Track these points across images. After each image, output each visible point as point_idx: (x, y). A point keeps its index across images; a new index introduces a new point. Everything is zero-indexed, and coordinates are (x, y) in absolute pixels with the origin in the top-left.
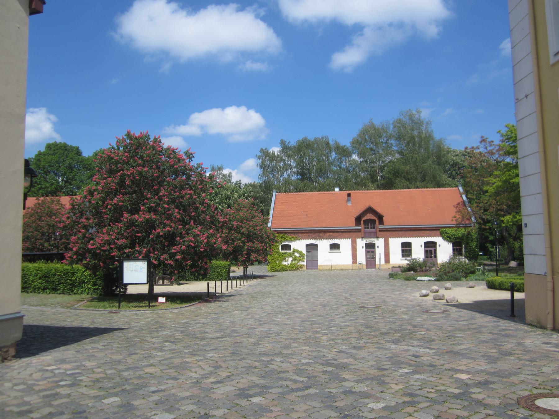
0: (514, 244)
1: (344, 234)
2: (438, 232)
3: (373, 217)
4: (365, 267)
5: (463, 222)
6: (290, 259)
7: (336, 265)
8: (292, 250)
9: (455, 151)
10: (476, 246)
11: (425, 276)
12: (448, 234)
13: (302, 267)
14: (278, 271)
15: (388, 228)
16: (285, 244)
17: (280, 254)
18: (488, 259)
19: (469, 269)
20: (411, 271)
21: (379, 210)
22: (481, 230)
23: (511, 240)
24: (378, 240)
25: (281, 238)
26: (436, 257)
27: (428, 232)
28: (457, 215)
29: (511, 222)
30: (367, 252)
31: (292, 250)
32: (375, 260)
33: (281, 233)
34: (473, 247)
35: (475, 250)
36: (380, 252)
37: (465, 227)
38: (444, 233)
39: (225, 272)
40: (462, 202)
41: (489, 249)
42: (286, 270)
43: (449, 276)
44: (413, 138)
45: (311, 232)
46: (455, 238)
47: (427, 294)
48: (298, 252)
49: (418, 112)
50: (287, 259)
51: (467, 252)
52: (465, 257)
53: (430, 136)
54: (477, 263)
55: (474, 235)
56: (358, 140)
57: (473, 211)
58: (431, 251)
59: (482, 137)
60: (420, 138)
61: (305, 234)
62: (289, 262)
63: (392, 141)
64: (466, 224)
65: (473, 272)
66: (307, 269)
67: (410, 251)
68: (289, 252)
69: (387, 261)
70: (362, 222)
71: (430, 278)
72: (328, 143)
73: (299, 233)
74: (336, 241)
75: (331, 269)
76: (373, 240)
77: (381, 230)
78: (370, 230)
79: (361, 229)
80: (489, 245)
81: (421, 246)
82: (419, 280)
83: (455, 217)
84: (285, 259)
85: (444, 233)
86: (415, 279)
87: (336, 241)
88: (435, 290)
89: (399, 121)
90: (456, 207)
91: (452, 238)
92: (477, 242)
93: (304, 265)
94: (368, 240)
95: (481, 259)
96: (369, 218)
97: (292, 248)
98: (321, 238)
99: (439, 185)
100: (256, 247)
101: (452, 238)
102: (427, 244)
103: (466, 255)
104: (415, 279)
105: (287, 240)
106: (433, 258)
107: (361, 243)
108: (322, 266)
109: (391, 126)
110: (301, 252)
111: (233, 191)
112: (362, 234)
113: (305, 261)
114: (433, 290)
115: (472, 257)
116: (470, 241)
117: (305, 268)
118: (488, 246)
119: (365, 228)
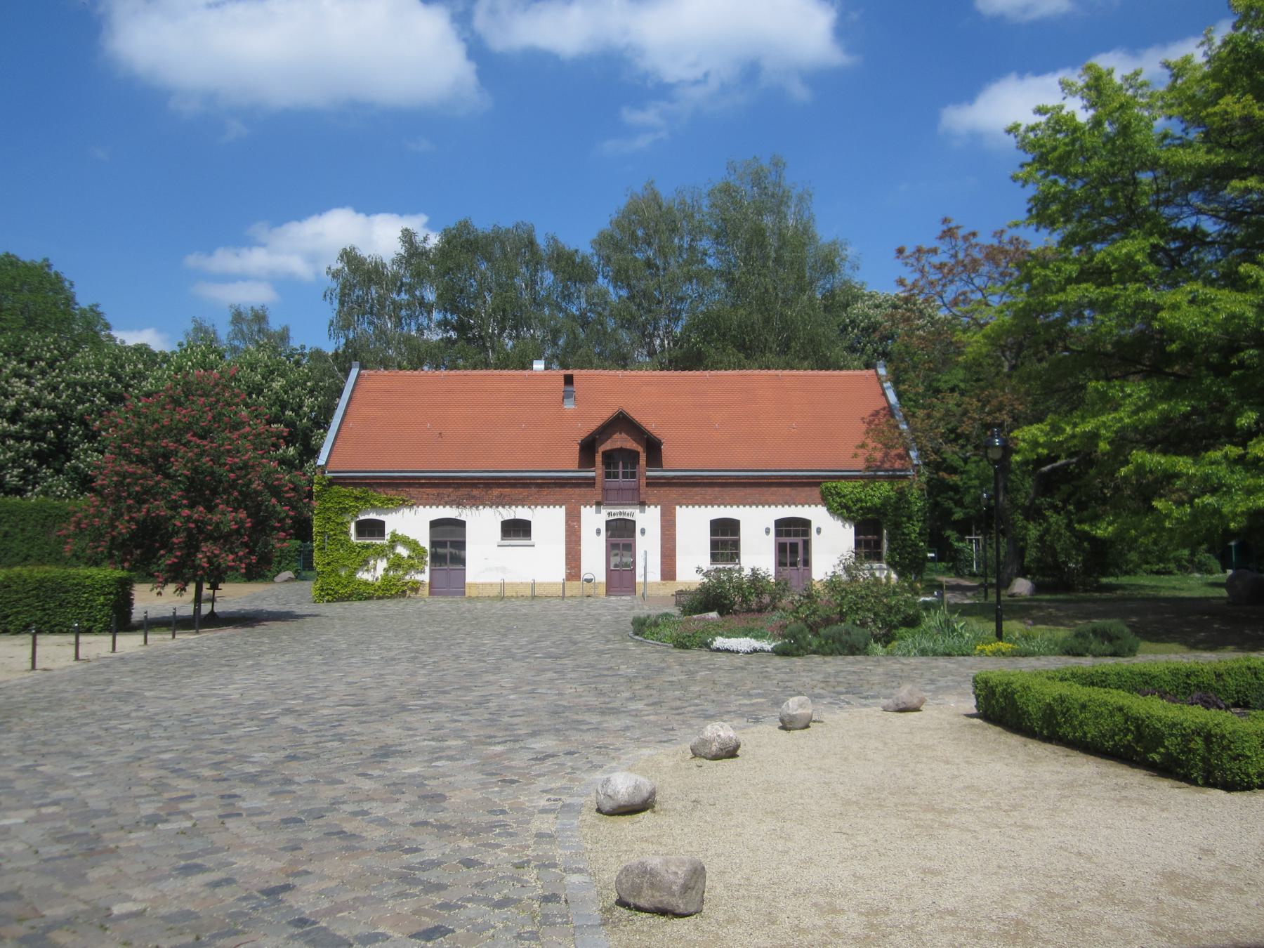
0: (1026, 528)
1: (545, 491)
2: (816, 492)
3: (630, 444)
4: (603, 590)
5: (887, 466)
6: (382, 565)
7: (517, 585)
8: (387, 537)
9: (872, 296)
10: (920, 534)
11: (746, 634)
12: (844, 496)
13: (416, 587)
14: (342, 599)
15: (673, 478)
16: (367, 517)
17: (352, 549)
18: (949, 569)
19: (898, 612)
20: (712, 610)
21: (651, 425)
22: (936, 488)
23: (1019, 518)
24: (643, 511)
25: (357, 499)
26: (807, 562)
27: (787, 490)
28: (869, 441)
29: (1043, 446)
30: (612, 547)
31: (387, 537)
32: (634, 569)
33: (356, 485)
34: (913, 536)
35: (917, 545)
36: (648, 547)
37: (891, 478)
38: (831, 494)
39: (103, 605)
40: (884, 409)
41: (951, 545)
42: (369, 598)
43: (827, 638)
44: (759, 232)
45: (448, 485)
46: (861, 508)
47: (638, 800)
48: (406, 542)
49: (776, 165)
50: (372, 562)
51: (895, 549)
52: (888, 563)
53: (806, 230)
54: (921, 582)
55: (917, 502)
56: (612, 237)
57: (913, 430)
58: (794, 547)
59: (945, 221)
60: (781, 235)
61: (428, 490)
62: (380, 572)
63: (705, 243)
64: (894, 470)
65: (912, 622)
66: (431, 593)
67: (736, 544)
68: (378, 542)
69: (668, 572)
70: (599, 458)
71: (757, 644)
72: (531, 243)
73: (410, 485)
74: (520, 513)
75: (502, 595)
76: (628, 510)
77: (653, 483)
78: (621, 481)
79: (593, 478)
80: (951, 534)
81: (768, 531)
82: (718, 650)
83: (863, 446)
84: (366, 562)
85: (831, 494)
86: (707, 645)
87: (520, 513)
88: (715, 747)
89: (727, 190)
90: (870, 423)
91: (854, 508)
92: (924, 521)
93: (422, 583)
94: (613, 511)
95: (932, 570)
96: (618, 445)
97: (388, 530)
98: (475, 502)
99: (824, 364)
100: (218, 524)
101: (854, 508)
102: (785, 527)
103: (893, 558)
104: (707, 645)
105: (373, 507)
106: (800, 566)
107: (594, 520)
108: (476, 585)
109: (705, 203)
110: (416, 543)
111: (272, 372)
112: (597, 493)
113: (427, 569)
114: (705, 742)
115: (909, 564)
116: (905, 519)
117: (425, 591)
118: (948, 537)
119: (608, 475)
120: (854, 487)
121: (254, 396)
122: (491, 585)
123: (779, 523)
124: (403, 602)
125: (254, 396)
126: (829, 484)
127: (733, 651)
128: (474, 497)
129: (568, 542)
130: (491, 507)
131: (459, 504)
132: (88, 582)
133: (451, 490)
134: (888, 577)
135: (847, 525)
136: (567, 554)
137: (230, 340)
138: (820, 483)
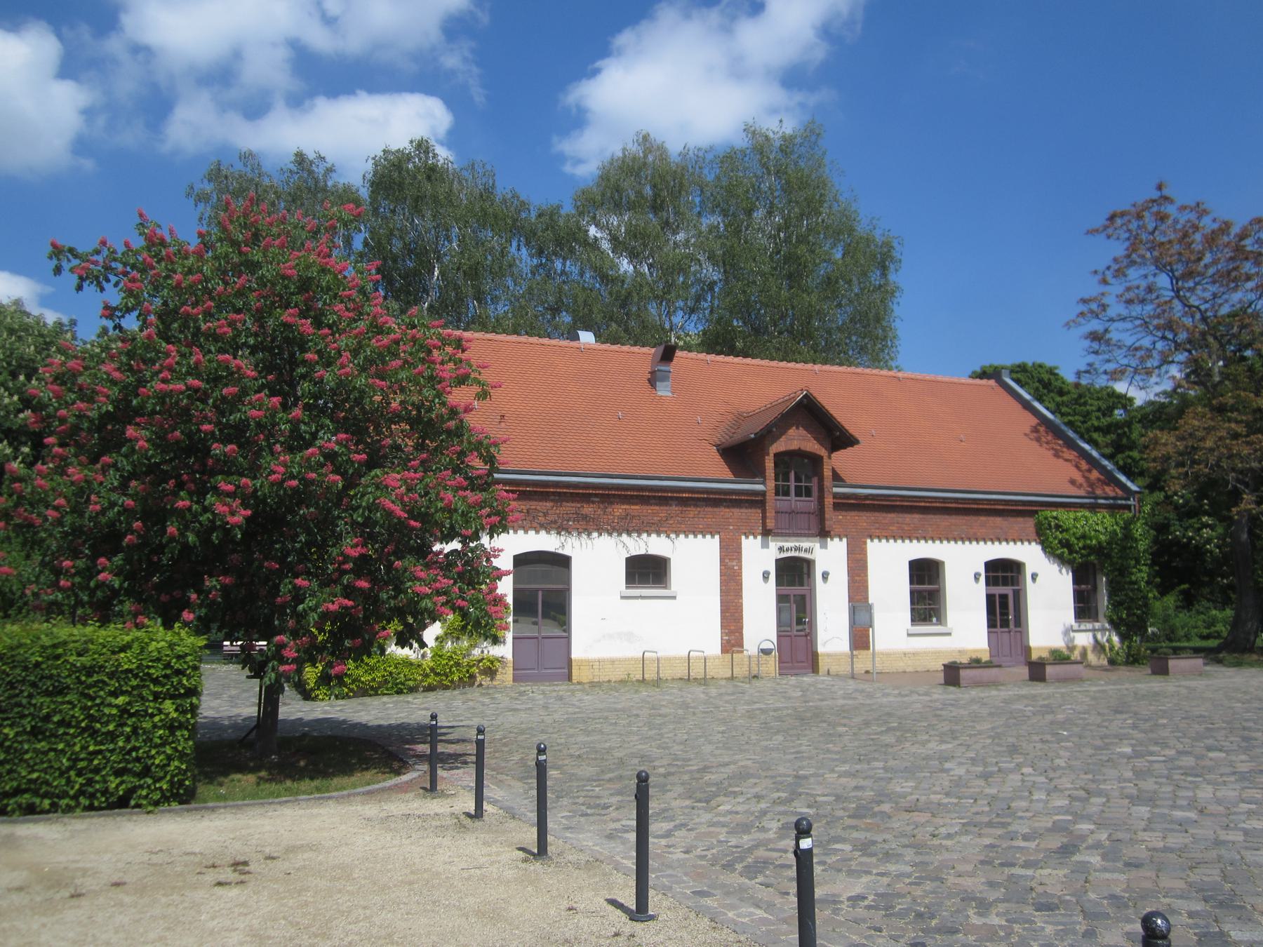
1: (692, 511)
2: (1029, 524)
12: (1067, 530)
15: (867, 497)
51: (1120, 604)
58: (1004, 597)
70: (769, 464)
74: (654, 545)
76: (805, 544)
79: (763, 494)
81: (766, 576)
87: (654, 545)
93: (501, 660)
94: (787, 545)
96: (794, 446)
98: (587, 526)
108: (590, 663)
116: (1133, 562)
117: (506, 676)
121: (22, 378)
122: (613, 661)
124: (474, 694)
125: (22, 378)
126: (1048, 513)
128: (585, 517)
129: (724, 593)
130: (610, 534)
131: (561, 528)
132: (127, 661)
133: (549, 504)
134: (1109, 641)
135: (1064, 570)
136: (722, 612)
138: (1036, 512)
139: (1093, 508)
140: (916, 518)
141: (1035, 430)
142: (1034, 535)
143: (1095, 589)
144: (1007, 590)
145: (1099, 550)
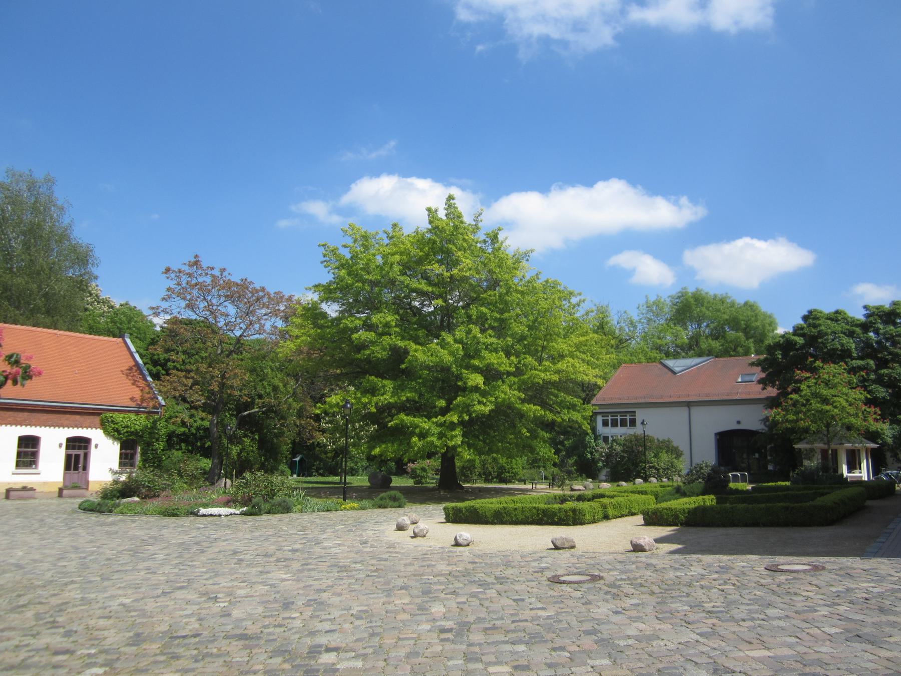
2: (97, 419)
5: (145, 404)
12: (117, 423)
26: (85, 468)
27: (78, 417)
46: (127, 432)
58: (77, 457)
81: (60, 445)
86: (196, 514)
120: (124, 418)
123: (69, 440)
126: (108, 415)
127: (216, 515)
137: (766, 426)
138: (101, 414)
139: (137, 413)
140: (26, 415)
141: (130, 369)
142: (99, 425)
143: (135, 453)
144: (81, 452)
145: (135, 433)
